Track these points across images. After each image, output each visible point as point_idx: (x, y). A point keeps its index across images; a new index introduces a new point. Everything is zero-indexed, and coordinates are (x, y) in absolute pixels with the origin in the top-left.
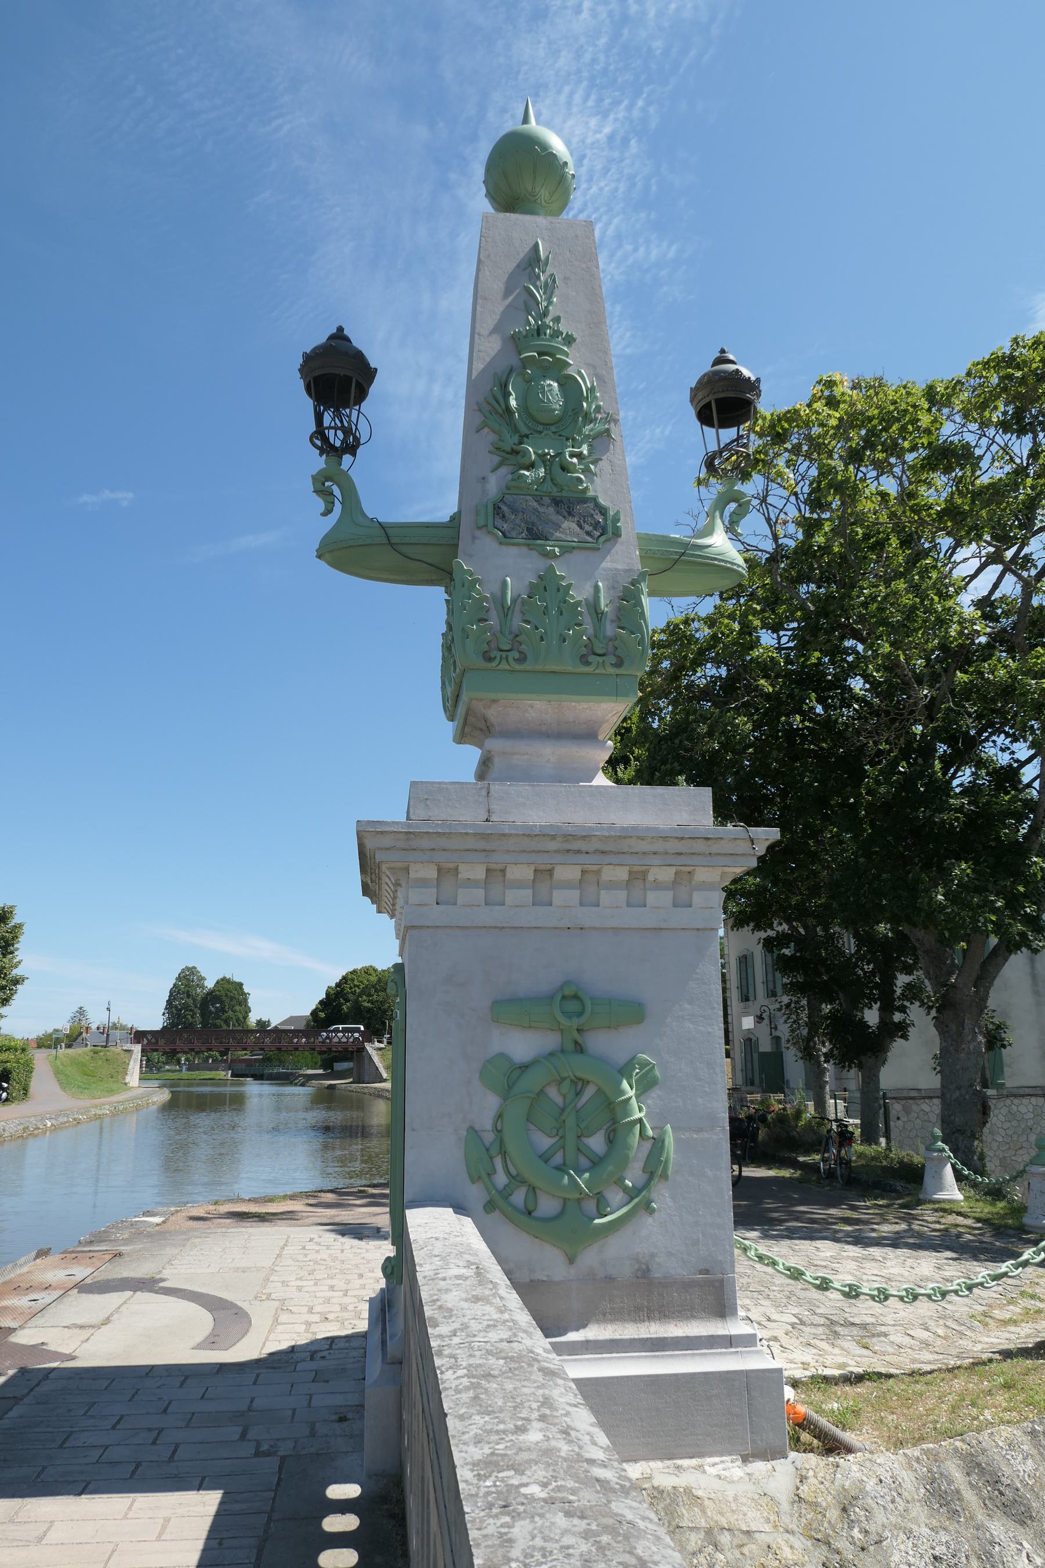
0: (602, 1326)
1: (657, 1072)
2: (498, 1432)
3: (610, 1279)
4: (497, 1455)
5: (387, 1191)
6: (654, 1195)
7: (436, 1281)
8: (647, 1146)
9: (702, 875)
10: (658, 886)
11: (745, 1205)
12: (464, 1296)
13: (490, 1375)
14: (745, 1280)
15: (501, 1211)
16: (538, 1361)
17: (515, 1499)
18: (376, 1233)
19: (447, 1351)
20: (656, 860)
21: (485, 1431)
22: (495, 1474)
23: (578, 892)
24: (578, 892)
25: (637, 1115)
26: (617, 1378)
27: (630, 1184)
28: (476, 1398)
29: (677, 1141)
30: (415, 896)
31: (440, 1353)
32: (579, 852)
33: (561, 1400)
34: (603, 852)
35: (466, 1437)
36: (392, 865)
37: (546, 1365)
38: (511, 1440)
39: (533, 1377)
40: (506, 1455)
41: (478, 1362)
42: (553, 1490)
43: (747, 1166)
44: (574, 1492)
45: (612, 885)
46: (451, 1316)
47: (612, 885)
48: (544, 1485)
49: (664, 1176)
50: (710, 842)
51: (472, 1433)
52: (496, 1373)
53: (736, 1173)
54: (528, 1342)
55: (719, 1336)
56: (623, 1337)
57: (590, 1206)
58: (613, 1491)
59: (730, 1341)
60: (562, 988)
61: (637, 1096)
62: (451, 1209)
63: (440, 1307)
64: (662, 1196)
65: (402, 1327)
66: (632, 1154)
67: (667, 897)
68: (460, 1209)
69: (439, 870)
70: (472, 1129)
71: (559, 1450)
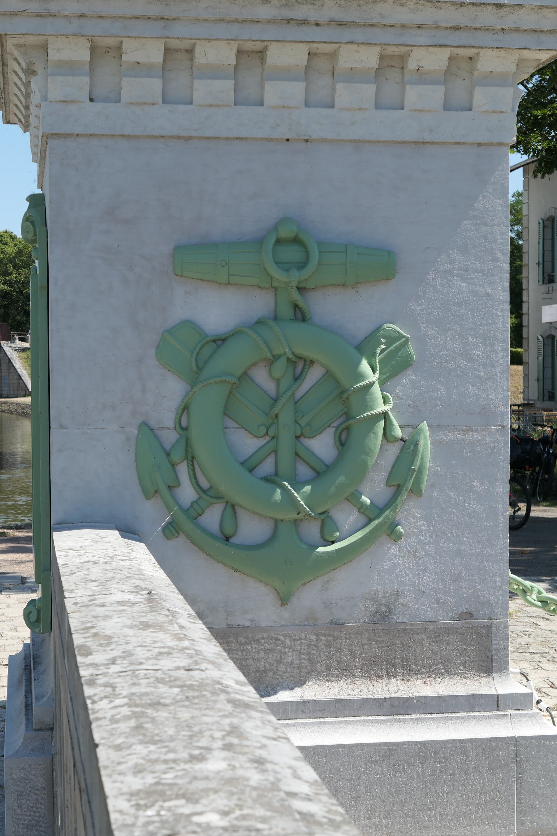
0: (325, 684)
1: (411, 349)
2: (166, 762)
3: (336, 624)
4: (164, 784)
5: (28, 519)
6: (400, 516)
7: (91, 608)
8: (394, 450)
9: (490, 62)
10: (422, 77)
11: (531, 552)
12: (129, 622)
13: (159, 703)
14: (524, 640)
15: (188, 537)
16: (228, 693)
17: (184, 827)
18: (21, 584)
19: (101, 680)
20: (421, 38)
21: (149, 761)
22: (160, 803)
23: (302, 86)
24: (302, 86)
25: (381, 408)
26: (343, 746)
27: (368, 502)
28: (139, 727)
29: (436, 443)
30: (58, 88)
31: (92, 682)
32: (304, 22)
33: (254, 732)
34: (341, 24)
35: (122, 767)
36: (22, 40)
37: (238, 697)
38: (184, 770)
39: (219, 706)
40: (175, 784)
41: (143, 690)
42: (237, 819)
43: (537, 504)
44: (264, 820)
45: (354, 76)
46: (109, 644)
47: (354, 76)
48: (225, 814)
49: (416, 491)
50: (503, 11)
51: (131, 764)
52: (168, 701)
53: (522, 513)
54: (213, 673)
55: (482, 696)
56: (352, 697)
57: (312, 530)
58: (320, 824)
59: (497, 703)
60: (276, 228)
61: (382, 383)
62: (116, 532)
63: (96, 635)
64: (411, 517)
65: (52, 685)
66: (371, 461)
67: (435, 94)
68: (129, 532)
69: (93, 49)
70: (145, 426)
71: (248, 779)
